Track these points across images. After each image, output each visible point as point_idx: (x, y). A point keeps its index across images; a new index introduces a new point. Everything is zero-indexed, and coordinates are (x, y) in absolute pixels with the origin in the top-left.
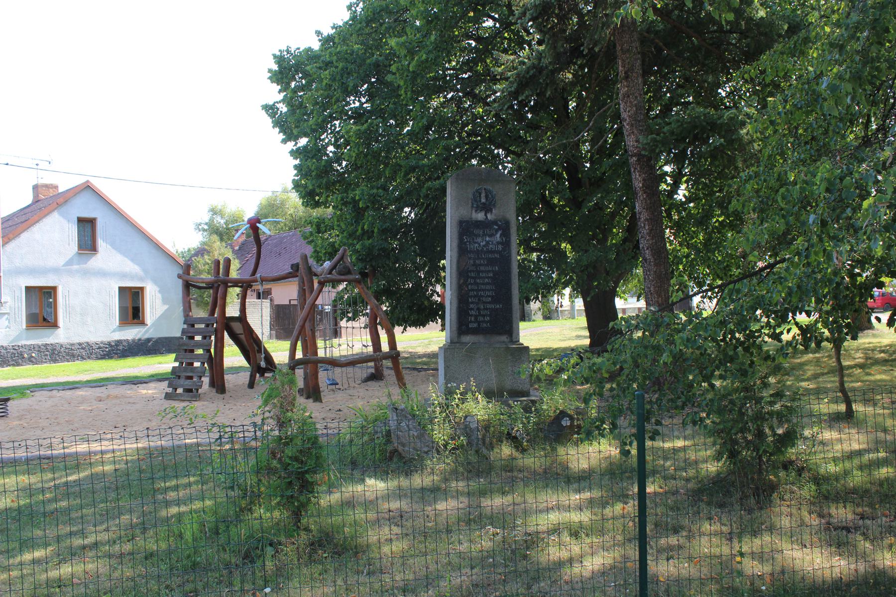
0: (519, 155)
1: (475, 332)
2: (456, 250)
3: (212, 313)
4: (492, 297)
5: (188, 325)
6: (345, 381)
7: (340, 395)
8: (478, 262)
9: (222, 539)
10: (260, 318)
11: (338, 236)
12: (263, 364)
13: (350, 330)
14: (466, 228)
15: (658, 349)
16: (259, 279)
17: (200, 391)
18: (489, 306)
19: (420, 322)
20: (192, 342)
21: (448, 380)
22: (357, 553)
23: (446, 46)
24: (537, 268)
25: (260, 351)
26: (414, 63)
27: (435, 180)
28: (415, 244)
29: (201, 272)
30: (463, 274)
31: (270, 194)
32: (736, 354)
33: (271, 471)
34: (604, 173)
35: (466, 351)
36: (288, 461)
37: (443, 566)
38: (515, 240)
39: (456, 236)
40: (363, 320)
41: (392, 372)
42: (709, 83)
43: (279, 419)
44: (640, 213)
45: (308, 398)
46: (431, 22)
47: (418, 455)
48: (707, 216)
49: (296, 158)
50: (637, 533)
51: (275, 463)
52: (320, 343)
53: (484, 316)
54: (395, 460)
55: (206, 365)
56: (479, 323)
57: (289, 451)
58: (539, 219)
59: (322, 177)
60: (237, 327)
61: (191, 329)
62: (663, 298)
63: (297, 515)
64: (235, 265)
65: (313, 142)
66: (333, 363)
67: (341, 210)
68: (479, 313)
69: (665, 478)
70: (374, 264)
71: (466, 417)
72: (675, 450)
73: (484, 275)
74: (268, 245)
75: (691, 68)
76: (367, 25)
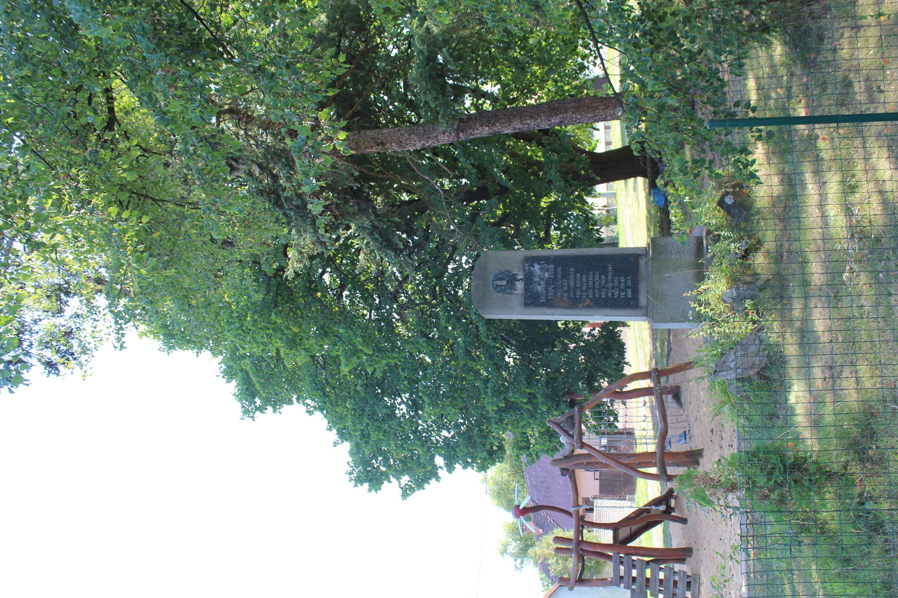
0: (455, 248)
1: (636, 291)
2: (553, 310)
3: (609, 557)
4: (601, 274)
5: (620, 582)
6: (680, 425)
7: (695, 431)
8: (565, 289)
9: (854, 553)
10: (612, 510)
11: (533, 429)
12: (662, 508)
13: (628, 419)
14: (532, 300)
15: (661, 108)
16: (576, 509)
17: (689, 574)
19: (621, 348)
20: (638, 580)
21: (686, 319)
22: (872, 414)
23: (349, 318)
24: (565, 230)
25: (648, 511)
26: (365, 350)
27: (478, 331)
28: (541, 352)
29: (565, 568)
30: (574, 303)
31: (488, 495)
32: (667, 28)
33: (782, 501)
34: (473, 165)
35: (656, 301)
36: (772, 483)
37: (888, 325)
38: (539, 252)
39: (539, 310)
40: (618, 406)
41: (672, 377)
42: (387, 65)
43: (728, 490)
44: (515, 129)
45: (698, 463)
46: (326, 332)
47: (764, 350)
48: (515, 62)
49: (454, 468)
50: (852, 124)
51: (774, 496)
52: (640, 449)
53: (620, 283)
54: (768, 374)
55: (662, 566)
56: (627, 287)
57: (761, 481)
58: (517, 229)
59: (475, 442)
60: (624, 533)
61: (625, 579)
62: (599, 104)
63: (830, 476)
64: (559, 532)
65: (440, 450)
66: (663, 437)
67: (507, 424)
69: (789, 97)
70: (562, 393)
71: (724, 301)
72: (759, 88)
73: (578, 282)
74: (538, 499)
75: (372, 83)
76: (328, 396)
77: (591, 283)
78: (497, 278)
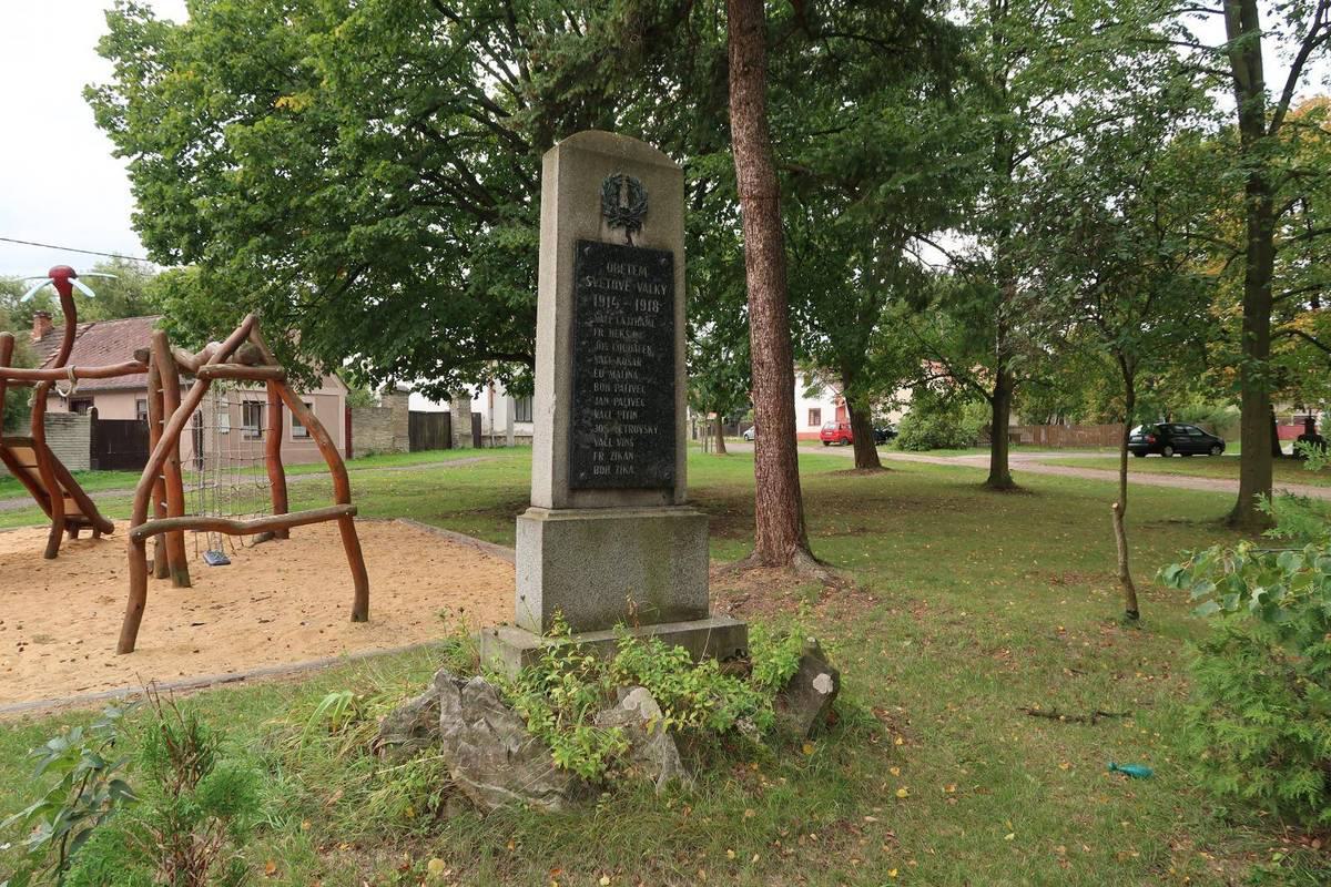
4: (639, 410)
16: (70, 374)
18: (634, 429)
53: (623, 450)
56: (614, 464)
68: (614, 443)
77: (623, 388)
78: (632, 185)
